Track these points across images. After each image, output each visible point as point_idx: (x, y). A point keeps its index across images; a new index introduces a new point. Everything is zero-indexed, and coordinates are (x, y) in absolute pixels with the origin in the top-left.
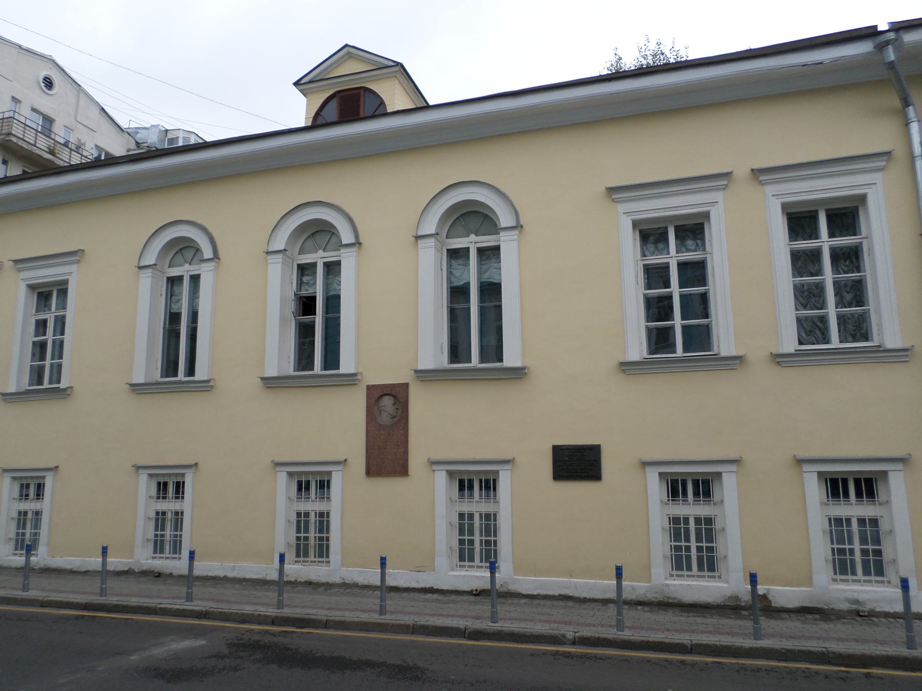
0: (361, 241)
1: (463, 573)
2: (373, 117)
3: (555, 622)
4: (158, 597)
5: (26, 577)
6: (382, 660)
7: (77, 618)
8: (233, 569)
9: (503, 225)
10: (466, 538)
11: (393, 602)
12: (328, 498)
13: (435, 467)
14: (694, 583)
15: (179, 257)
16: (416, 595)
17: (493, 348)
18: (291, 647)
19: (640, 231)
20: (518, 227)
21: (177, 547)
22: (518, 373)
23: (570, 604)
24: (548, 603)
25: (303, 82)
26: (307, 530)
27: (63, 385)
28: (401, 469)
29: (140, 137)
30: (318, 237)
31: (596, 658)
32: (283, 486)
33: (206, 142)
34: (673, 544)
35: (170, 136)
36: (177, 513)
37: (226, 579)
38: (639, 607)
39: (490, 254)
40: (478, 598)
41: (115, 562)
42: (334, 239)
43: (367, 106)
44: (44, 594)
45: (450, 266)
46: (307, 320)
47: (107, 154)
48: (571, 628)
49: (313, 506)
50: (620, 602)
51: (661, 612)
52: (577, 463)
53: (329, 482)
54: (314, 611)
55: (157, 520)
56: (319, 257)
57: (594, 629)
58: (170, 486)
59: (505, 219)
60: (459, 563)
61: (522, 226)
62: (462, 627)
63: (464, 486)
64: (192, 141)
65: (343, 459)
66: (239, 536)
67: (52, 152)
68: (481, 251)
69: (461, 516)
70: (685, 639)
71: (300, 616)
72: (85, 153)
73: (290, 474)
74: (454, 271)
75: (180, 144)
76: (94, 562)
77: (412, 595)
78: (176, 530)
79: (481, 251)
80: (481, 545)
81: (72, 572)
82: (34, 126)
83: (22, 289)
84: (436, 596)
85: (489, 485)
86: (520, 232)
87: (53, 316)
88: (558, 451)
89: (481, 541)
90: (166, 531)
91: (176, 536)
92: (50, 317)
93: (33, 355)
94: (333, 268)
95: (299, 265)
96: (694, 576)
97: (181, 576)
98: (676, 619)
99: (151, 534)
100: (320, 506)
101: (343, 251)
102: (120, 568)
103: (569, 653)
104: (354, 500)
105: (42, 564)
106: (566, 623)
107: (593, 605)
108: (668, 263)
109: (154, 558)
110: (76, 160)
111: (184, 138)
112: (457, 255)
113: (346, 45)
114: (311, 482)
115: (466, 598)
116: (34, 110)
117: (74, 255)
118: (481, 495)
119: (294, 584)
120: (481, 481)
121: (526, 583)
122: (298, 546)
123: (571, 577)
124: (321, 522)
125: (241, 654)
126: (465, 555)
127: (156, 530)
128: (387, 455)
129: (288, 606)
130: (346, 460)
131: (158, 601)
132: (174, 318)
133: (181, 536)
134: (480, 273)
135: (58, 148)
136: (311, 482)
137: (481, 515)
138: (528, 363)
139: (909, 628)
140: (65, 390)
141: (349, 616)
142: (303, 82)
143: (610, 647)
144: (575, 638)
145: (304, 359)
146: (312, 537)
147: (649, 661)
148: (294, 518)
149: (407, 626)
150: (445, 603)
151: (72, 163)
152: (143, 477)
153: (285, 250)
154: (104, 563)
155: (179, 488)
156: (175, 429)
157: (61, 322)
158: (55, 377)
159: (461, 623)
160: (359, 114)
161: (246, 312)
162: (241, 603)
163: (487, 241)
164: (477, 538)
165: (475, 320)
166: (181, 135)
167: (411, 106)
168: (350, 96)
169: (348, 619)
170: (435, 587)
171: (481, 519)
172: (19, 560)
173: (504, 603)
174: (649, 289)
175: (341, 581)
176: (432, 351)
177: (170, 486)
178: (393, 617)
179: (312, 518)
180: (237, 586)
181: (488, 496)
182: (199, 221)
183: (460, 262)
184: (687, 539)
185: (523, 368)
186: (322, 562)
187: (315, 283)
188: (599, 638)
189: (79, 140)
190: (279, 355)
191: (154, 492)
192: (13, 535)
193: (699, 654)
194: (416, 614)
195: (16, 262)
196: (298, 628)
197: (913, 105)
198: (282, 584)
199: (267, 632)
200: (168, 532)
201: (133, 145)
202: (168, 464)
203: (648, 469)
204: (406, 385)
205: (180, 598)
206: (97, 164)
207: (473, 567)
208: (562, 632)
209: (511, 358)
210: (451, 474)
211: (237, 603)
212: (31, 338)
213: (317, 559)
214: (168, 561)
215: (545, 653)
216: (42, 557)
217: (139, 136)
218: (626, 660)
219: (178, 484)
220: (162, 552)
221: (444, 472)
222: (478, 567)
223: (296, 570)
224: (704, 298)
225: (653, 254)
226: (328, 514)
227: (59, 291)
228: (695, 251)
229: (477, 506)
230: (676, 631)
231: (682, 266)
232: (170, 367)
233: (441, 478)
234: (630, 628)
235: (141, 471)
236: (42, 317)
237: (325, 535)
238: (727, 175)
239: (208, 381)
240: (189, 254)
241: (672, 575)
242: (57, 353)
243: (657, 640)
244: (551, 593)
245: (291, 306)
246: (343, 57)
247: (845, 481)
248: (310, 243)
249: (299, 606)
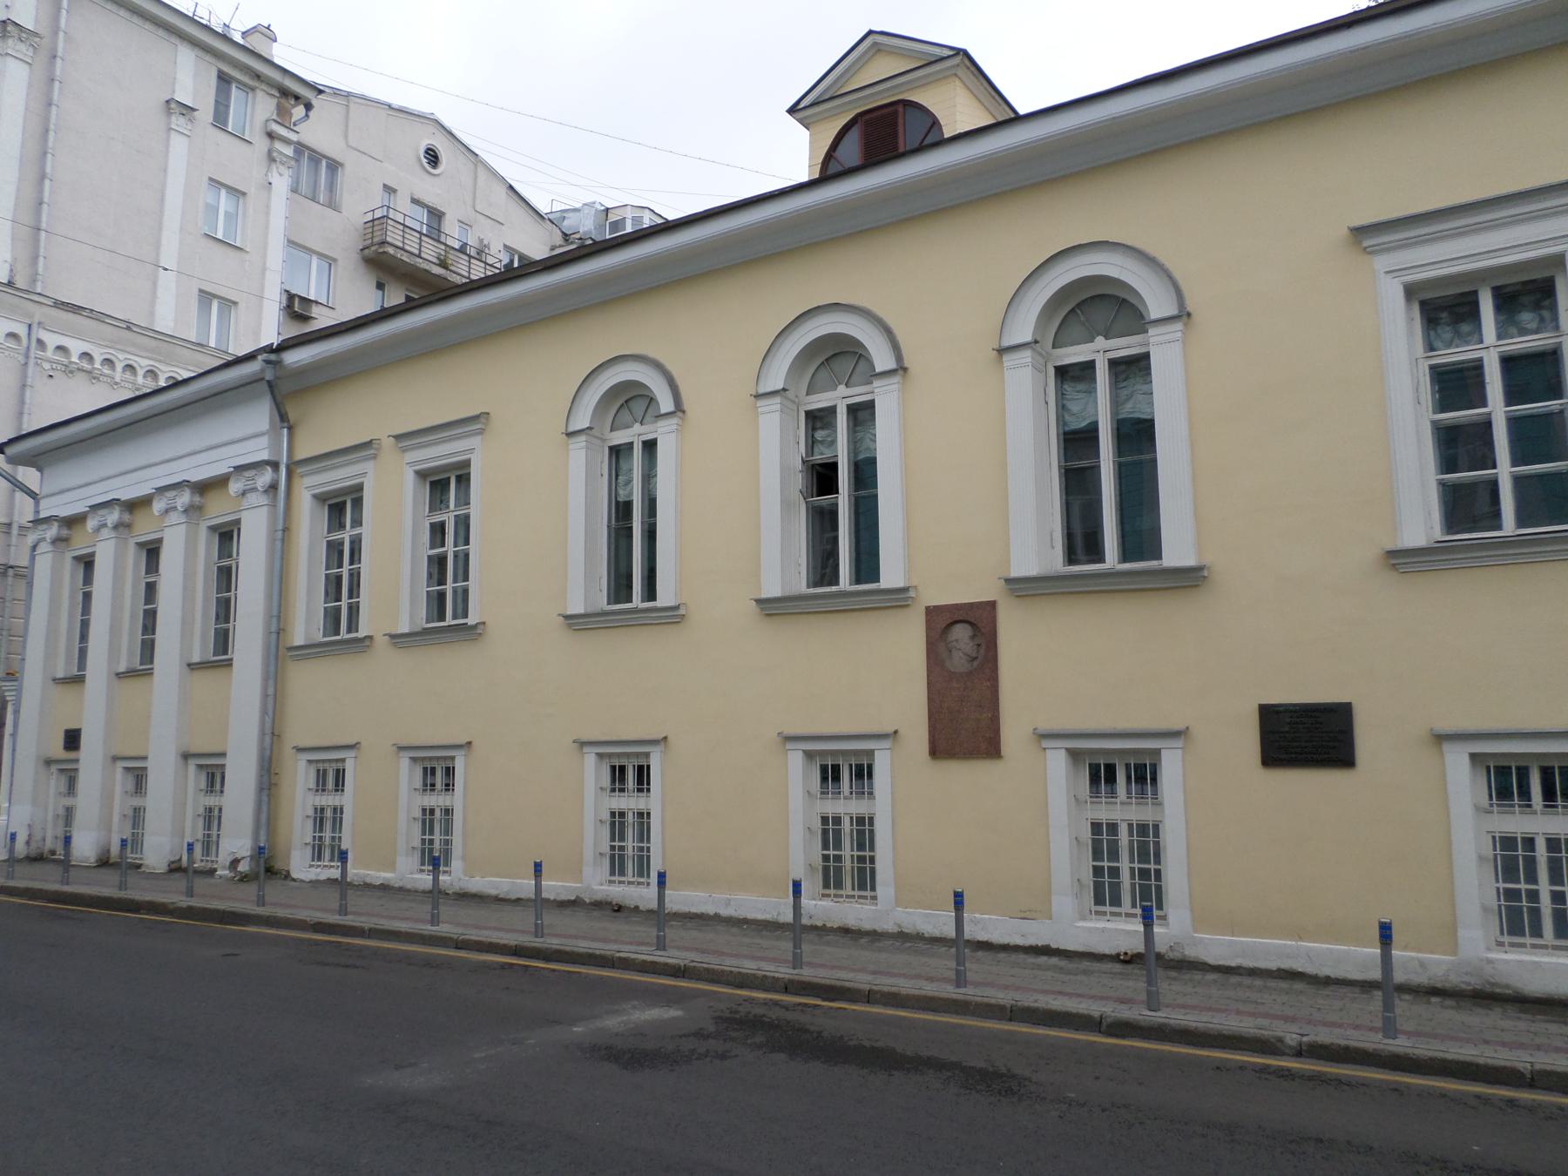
0: (906, 364)
1: (1101, 924)
2: (920, 149)
3: (1266, 1015)
4: (616, 941)
5: (435, 906)
6: (953, 1059)
7: (503, 966)
8: (728, 903)
9: (1154, 315)
10: (1106, 864)
11: (977, 967)
12: (871, 793)
13: (1045, 744)
14: (1554, 960)
15: (625, 414)
16: (1021, 957)
17: (1141, 537)
18: (812, 1028)
19: (1423, 304)
20: (1183, 315)
21: (643, 866)
22: (1190, 578)
23: (1299, 986)
24: (1258, 982)
25: (802, 105)
26: (838, 845)
27: (471, 621)
28: (987, 745)
29: (567, 225)
30: (837, 365)
31: (1339, 1082)
32: (798, 774)
33: (667, 221)
34: (1502, 885)
35: (613, 218)
36: (641, 814)
37: (717, 918)
38: (1434, 999)
39: (1133, 368)
40: (1130, 967)
41: (555, 887)
42: (862, 366)
43: (910, 133)
44: (460, 930)
45: (1061, 395)
46: (824, 503)
47: (522, 257)
48: (1295, 1028)
49: (846, 806)
50: (1386, 988)
51: (1480, 1010)
52: (1307, 737)
53: (870, 767)
54: (850, 976)
55: (613, 824)
56: (839, 397)
57: (1337, 1031)
58: (629, 772)
59: (1157, 303)
60: (1094, 908)
61: (1189, 315)
62: (1096, 1014)
63: (1102, 775)
64: (646, 223)
65: (890, 730)
66: (736, 850)
67: (443, 264)
68: (853, 410)
69: (1096, 827)
70: (1522, 1060)
71: (828, 982)
72: (490, 260)
73: (809, 755)
74: (1069, 405)
75: (629, 229)
76: (524, 886)
77: (1014, 957)
78: (642, 841)
79: (853, 410)
80: (1133, 877)
81: (498, 900)
82: (417, 226)
83: (410, 476)
84: (1054, 960)
85: (1145, 775)
86: (1186, 325)
87: (452, 515)
88: (1270, 716)
89: (1132, 869)
90: (627, 840)
91: (641, 849)
92: (449, 518)
93: (430, 576)
94: (862, 414)
95: (808, 413)
96: (1545, 947)
97: (651, 911)
98: (1508, 1024)
99: (605, 847)
100: (857, 807)
101: (876, 383)
102: (564, 897)
103: (1289, 1070)
104: (911, 797)
105: (456, 888)
106: (1286, 1019)
107: (1344, 990)
108: (1481, 360)
109: (611, 882)
110: (478, 272)
111: (634, 219)
112: (1074, 376)
113: (870, 32)
115: (1108, 966)
116: (415, 201)
117: (475, 422)
118: (1129, 792)
119: (821, 931)
120: (1128, 766)
121: (1216, 947)
122: (826, 870)
123: (1301, 939)
124: (861, 833)
125: (734, 1034)
126: (1105, 893)
127: (613, 839)
128: (964, 720)
129: (810, 964)
130: (896, 732)
131: (615, 947)
132: (623, 510)
133: (872, 860)
134: (1116, 403)
135: (452, 256)
136: (843, 769)
137: (1130, 826)
138: (1208, 559)
139: (343, 897)
140: (475, 627)
141: (906, 986)
142: (802, 105)
143: (1369, 1065)
144: (1300, 1044)
145: (824, 567)
146: (848, 856)
147: (1443, 1095)
148: (817, 825)
149: (1002, 1008)
150: (1069, 973)
151: (474, 277)
152: (590, 759)
153: (784, 390)
154: (538, 887)
155: (643, 774)
156: (629, 685)
157: (463, 523)
158: (460, 611)
159: (1094, 1009)
160: (896, 148)
161: (731, 496)
162: (737, 956)
163: (1125, 346)
164: (1124, 865)
165: (1108, 492)
166: (629, 214)
167: (987, 120)
168: (880, 119)
169: (904, 991)
170: (1054, 946)
171: (1131, 834)
172: (425, 880)
173: (1175, 979)
174: (1443, 411)
175: (896, 930)
176: (1036, 544)
177: (629, 772)
178: (978, 991)
179: (846, 825)
180: (734, 930)
181: (1143, 793)
182: (651, 354)
183: (1081, 386)
184: (1532, 877)
185: (1199, 569)
186: (865, 897)
187: (834, 442)
188: (1347, 1048)
189: (481, 241)
190: (781, 562)
191: (606, 780)
192: (417, 843)
193: (1549, 1089)
194: (1018, 988)
195: (398, 437)
196: (825, 1000)
198: (798, 930)
199: (776, 1003)
200: (630, 844)
201: (559, 240)
202: (624, 737)
203: (1447, 747)
204: (992, 605)
205: (647, 944)
206: (509, 275)
207: (1119, 914)
208: (1280, 1034)
209: (1176, 550)
210: (1074, 755)
211: (731, 955)
212: (426, 551)
213: (856, 893)
214: (632, 888)
215: (1242, 1067)
216: (456, 876)
217: (566, 223)
218: (1396, 1089)
219: (640, 768)
220: (622, 873)
221: (1063, 752)
222: (1127, 915)
223: (820, 907)
224: (1448, 463)
225: (1449, 345)
226: (871, 819)
227: (459, 478)
228: (1536, 332)
229: (1123, 810)
230: (1504, 1044)
231: (1509, 363)
232: (620, 587)
233: (1057, 762)
234: (1409, 1034)
235: (586, 749)
236: (437, 519)
237: (867, 854)
238: (367, 445)
239: (677, 608)
240: (638, 407)
241: (1501, 944)
242: (461, 572)
243: (1461, 1058)
244: (1262, 965)
245: (798, 481)
246: (865, 52)
247: (1523, 773)
248: (823, 374)
249: (824, 966)
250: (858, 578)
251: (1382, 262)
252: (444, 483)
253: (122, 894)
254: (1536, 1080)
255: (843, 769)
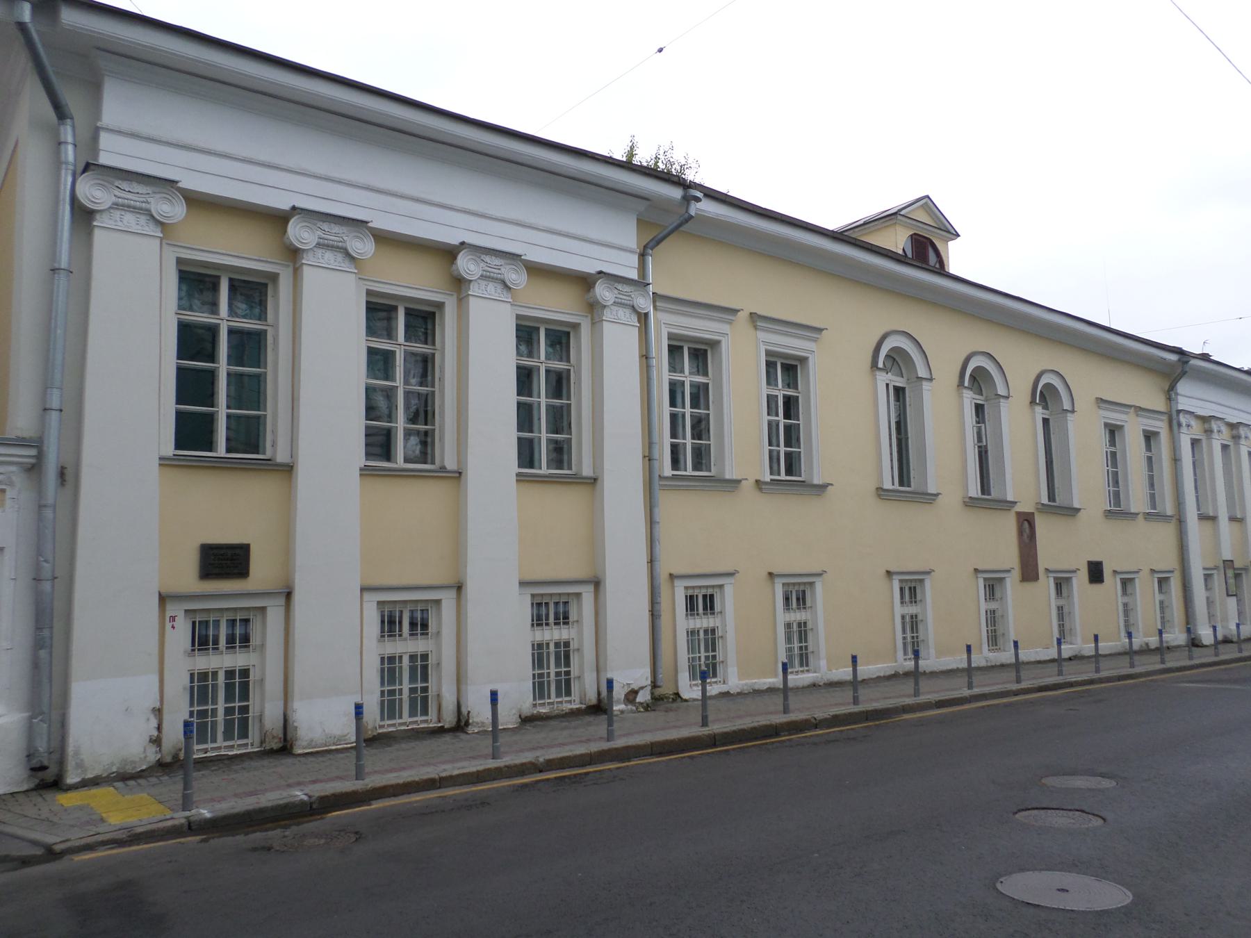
5: (1097, 662)
58: (911, 590)
114: (993, 587)
154: (1097, 648)
156: (705, 531)
197: (72, 118)
214: (801, 676)
223: (799, 678)
224: (259, 380)
250: (697, 467)
251: (762, 336)
252: (787, 369)
253: (705, 731)
254: (551, 765)
255: (993, 587)
